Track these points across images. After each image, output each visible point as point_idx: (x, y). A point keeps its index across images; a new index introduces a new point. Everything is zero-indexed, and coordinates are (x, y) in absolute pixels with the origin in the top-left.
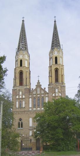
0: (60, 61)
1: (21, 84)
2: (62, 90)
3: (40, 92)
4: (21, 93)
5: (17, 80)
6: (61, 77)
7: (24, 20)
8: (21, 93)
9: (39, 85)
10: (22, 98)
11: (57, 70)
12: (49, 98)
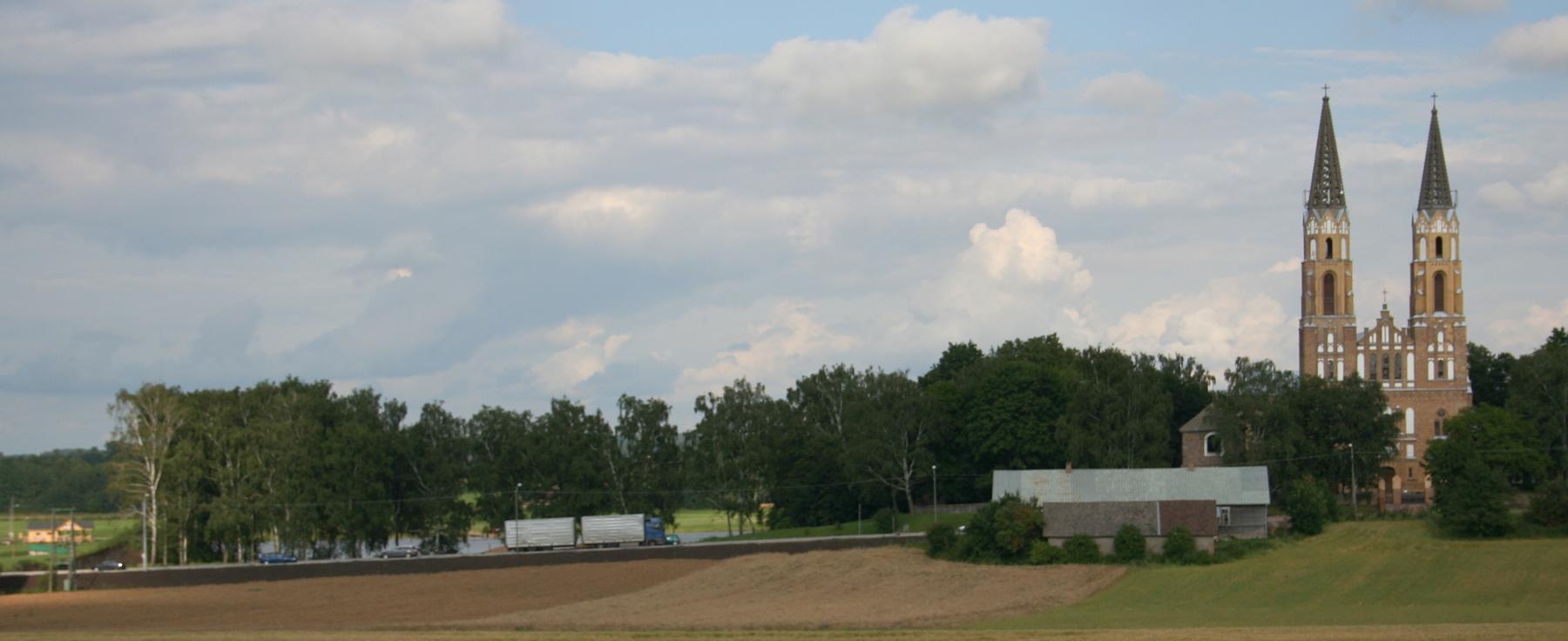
0: (1341, 251)
1: (1329, 308)
2: (1458, 337)
3: (1391, 337)
4: (1330, 338)
5: (1317, 299)
6: (1452, 300)
7: (1328, 95)
8: (1330, 338)
9: (1386, 319)
10: (1445, 353)
11: (1329, 279)
12: (1417, 358)
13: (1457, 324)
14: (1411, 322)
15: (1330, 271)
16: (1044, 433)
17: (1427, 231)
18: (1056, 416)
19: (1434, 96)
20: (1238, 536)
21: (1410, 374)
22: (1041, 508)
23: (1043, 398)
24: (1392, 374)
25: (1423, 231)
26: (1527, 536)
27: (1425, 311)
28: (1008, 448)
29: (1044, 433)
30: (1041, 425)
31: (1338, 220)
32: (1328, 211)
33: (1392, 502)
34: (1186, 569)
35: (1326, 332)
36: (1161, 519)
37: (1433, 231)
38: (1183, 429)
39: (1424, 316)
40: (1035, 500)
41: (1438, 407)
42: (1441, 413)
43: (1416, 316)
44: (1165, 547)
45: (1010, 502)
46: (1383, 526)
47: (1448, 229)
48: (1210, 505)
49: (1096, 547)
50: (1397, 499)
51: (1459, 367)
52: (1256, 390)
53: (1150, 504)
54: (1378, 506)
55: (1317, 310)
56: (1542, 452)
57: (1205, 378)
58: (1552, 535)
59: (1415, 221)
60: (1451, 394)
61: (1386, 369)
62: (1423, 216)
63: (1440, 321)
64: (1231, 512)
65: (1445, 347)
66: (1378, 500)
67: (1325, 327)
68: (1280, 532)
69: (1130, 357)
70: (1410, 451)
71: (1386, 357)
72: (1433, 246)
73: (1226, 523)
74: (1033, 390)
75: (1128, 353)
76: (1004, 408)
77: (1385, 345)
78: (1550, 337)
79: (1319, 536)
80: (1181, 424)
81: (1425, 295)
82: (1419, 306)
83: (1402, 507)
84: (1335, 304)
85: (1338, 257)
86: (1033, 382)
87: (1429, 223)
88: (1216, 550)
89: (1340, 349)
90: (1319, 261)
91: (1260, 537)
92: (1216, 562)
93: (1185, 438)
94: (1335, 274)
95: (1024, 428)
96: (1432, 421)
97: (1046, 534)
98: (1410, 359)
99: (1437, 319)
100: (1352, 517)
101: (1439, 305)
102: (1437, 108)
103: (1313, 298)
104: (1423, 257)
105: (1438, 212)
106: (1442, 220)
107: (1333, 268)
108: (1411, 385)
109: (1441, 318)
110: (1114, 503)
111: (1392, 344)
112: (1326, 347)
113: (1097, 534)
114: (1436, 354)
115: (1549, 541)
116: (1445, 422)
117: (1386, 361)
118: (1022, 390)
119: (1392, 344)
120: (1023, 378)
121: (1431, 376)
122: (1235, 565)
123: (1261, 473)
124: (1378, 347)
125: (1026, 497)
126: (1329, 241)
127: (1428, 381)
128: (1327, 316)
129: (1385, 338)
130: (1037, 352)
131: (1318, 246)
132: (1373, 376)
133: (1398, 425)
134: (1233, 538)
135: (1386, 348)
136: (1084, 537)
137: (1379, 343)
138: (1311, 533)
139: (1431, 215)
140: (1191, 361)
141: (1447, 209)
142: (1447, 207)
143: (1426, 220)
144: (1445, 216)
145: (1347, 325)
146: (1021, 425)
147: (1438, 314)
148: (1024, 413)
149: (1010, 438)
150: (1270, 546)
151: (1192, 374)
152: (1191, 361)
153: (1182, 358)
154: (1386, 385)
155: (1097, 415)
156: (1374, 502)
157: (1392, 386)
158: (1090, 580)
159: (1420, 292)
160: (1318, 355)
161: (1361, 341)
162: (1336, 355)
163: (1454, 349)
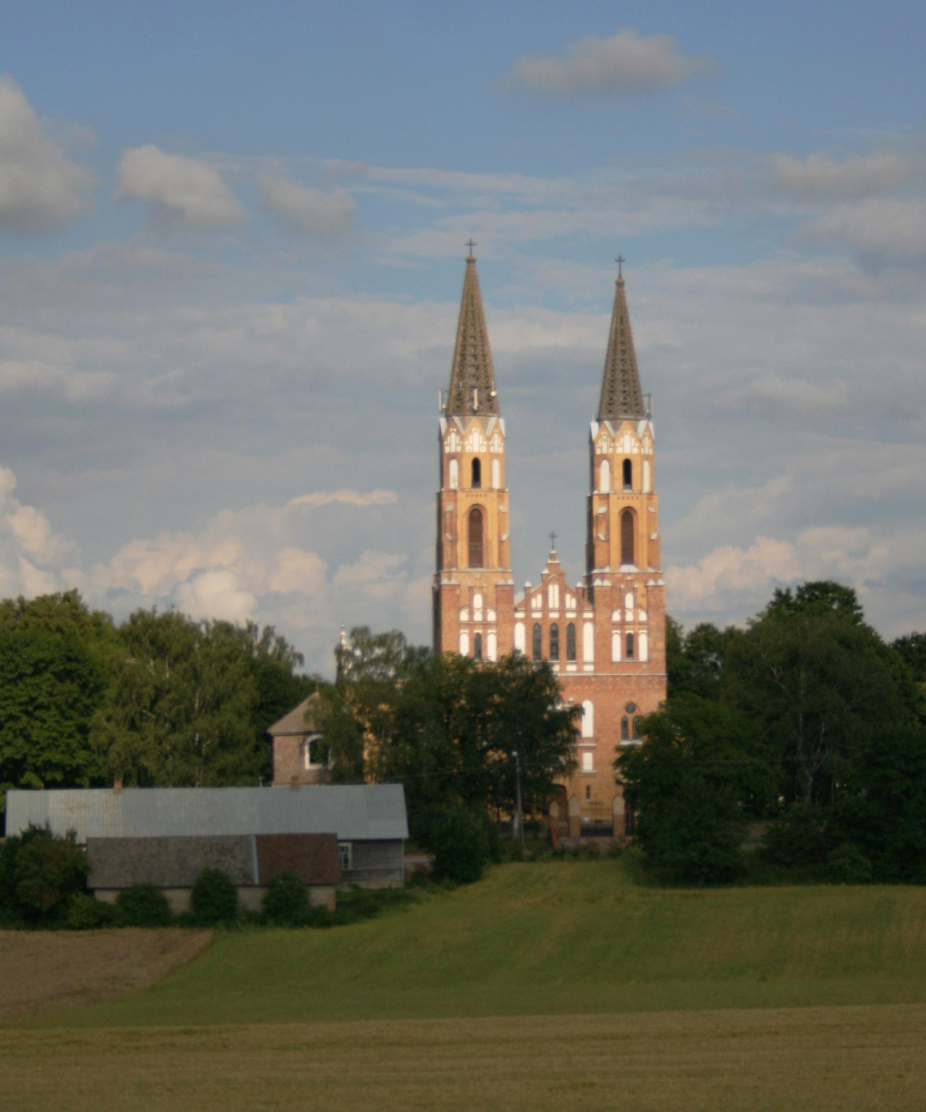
3: (562, 601)
4: (478, 600)
7: (476, 255)
8: (478, 600)
10: (637, 623)
13: (651, 583)
14: (589, 579)
15: (476, 504)
16: (70, 736)
17: (611, 450)
18: (87, 711)
19: (620, 260)
20: (363, 885)
21: (588, 651)
22: (81, 845)
23: (68, 683)
24: (563, 652)
25: (605, 451)
26: (766, 882)
27: (608, 563)
28: (18, 757)
29: (70, 736)
30: (66, 723)
31: (489, 432)
32: (474, 421)
33: (568, 834)
34: (299, 934)
35: (471, 590)
36: (260, 860)
37: (619, 450)
38: (274, 729)
39: (607, 570)
40: (72, 834)
41: (627, 700)
42: (631, 707)
43: (596, 571)
44: (266, 902)
45: (38, 837)
46: (566, 870)
47: (640, 448)
48: (327, 841)
49: (164, 902)
50: (575, 831)
51: (655, 643)
52: (380, 674)
53: (241, 840)
54: (549, 840)
55: (459, 561)
56: (772, 764)
57: (289, 657)
58: (799, 880)
59: (594, 436)
60: (644, 682)
61: (554, 645)
62: (455, 426)
63: (629, 578)
64: (354, 850)
65: (636, 615)
66: (549, 831)
67: (471, 584)
68: (417, 878)
69: (199, 626)
70: (587, 761)
71: (554, 628)
72: (619, 472)
73: (347, 867)
74: (54, 673)
75: (196, 619)
76: (13, 698)
77: (553, 610)
78: (772, 603)
79: (478, 884)
80: (271, 722)
81: (608, 541)
82: (599, 556)
83: (583, 841)
84: (484, 552)
85: (488, 485)
86: (52, 661)
87: (614, 440)
88: (338, 904)
89: (492, 616)
90: (462, 490)
91: (394, 886)
92: (340, 922)
93: (277, 741)
94: (485, 509)
95: (41, 728)
96: (618, 719)
97: (92, 883)
98: (587, 634)
99: (624, 574)
100: (517, 856)
101: (628, 556)
102: (625, 277)
103: (454, 542)
104: (604, 486)
105: (625, 424)
106: (632, 436)
107: (481, 500)
108: (589, 669)
109: (630, 574)
110: (191, 837)
111: (562, 610)
112: (471, 613)
113: (166, 884)
114: (623, 624)
115: (798, 889)
116: (639, 718)
117: (554, 633)
118: (38, 671)
119: (562, 610)
120: (41, 655)
121: (617, 654)
122: (368, 927)
123: (395, 793)
124: (544, 614)
125: (59, 830)
126: (476, 464)
127: (613, 663)
128: (474, 570)
129: (554, 601)
130: (50, 617)
131: (460, 469)
132: (537, 653)
133: (575, 723)
134: (356, 887)
135: (554, 616)
136: (149, 888)
137: (545, 609)
138: (468, 880)
139: (616, 427)
140: (269, 632)
141: (638, 420)
142: (639, 417)
143: (609, 435)
144: (635, 429)
145: (501, 582)
146: (37, 724)
147: (626, 568)
148: (41, 707)
149: (20, 741)
150: (409, 899)
151: (270, 651)
152: (269, 632)
153: (256, 628)
154: (556, 668)
155: (151, 709)
156: (542, 835)
157: (563, 669)
158: (163, 952)
159: (602, 536)
160: (460, 625)
161: (520, 605)
162: (485, 624)
163: (649, 617)
